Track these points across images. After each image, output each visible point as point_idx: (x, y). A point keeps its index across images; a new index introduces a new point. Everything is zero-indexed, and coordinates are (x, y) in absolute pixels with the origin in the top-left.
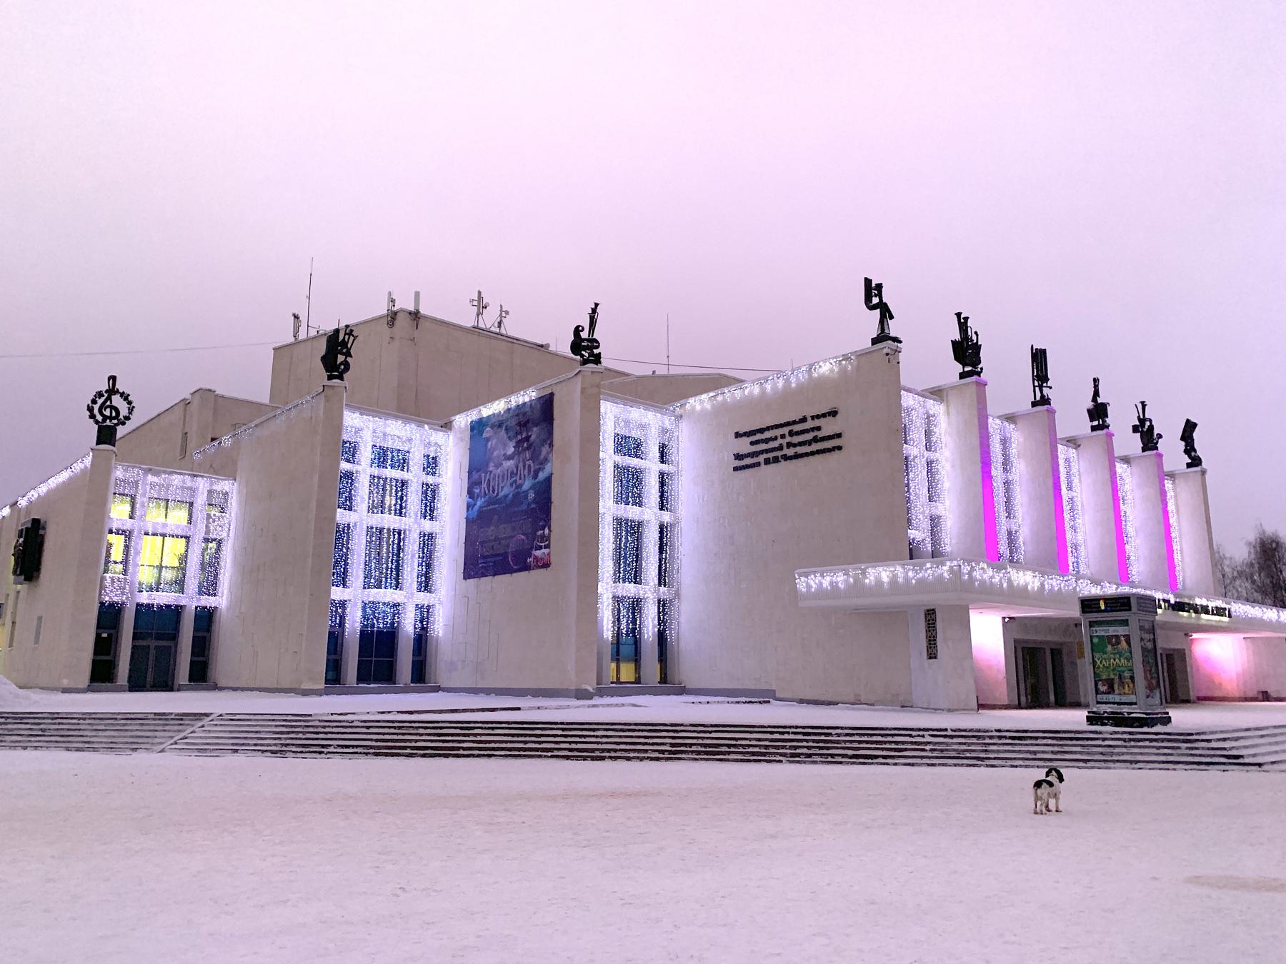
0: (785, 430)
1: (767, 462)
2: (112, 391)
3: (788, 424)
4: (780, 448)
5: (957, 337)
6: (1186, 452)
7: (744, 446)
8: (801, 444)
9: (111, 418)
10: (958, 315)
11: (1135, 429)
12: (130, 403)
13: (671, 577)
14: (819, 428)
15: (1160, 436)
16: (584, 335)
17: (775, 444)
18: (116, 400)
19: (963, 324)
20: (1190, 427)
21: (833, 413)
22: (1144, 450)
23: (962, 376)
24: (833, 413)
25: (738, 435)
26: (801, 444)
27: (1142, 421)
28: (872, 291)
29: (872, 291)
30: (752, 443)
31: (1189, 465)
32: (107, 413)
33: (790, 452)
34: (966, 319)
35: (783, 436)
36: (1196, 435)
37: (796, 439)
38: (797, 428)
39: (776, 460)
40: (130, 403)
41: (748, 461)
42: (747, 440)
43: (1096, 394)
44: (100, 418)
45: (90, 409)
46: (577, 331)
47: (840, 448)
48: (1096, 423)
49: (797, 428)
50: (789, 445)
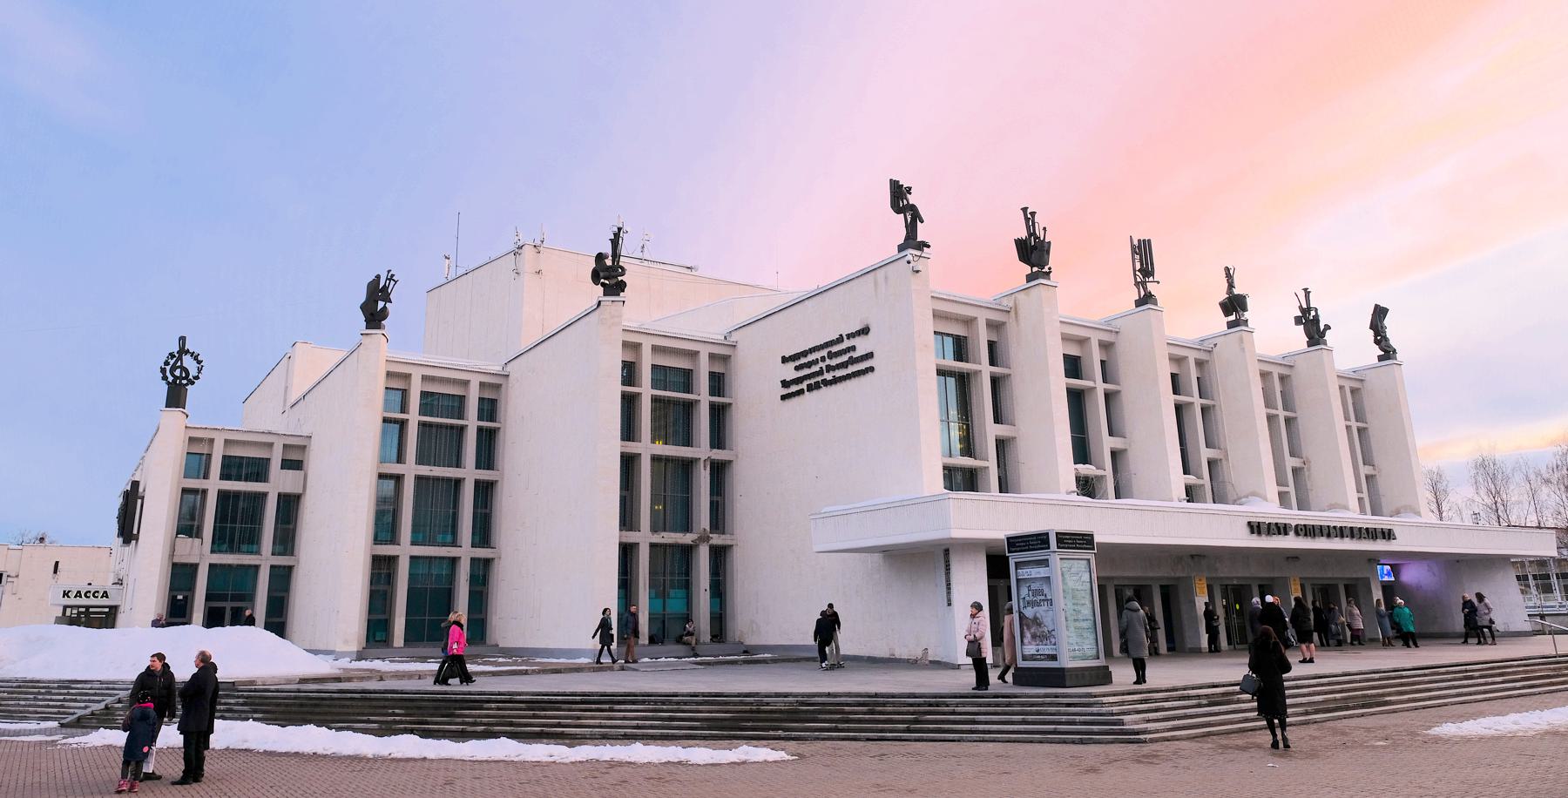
0: (824, 353)
1: (810, 388)
2: (183, 351)
3: (827, 345)
4: (820, 372)
5: (1023, 234)
6: (1377, 342)
7: (789, 372)
8: (839, 366)
9: (181, 378)
10: (1025, 210)
11: (1298, 321)
12: (199, 362)
13: (1312, 496)
14: (853, 348)
15: (1327, 327)
16: (609, 262)
17: (815, 369)
18: (188, 361)
19: (1029, 217)
20: (1380, 313)
21: (865, 331)
22: (1310, 344)
23: (1030, 278)
24: (865, 331)
25: (785, 360)
26: (839, 366)
27: (1306, 311)
28: (898, 193)
29: (898, 193)
30: (797, 368)
31: (1381, 358)
32: (177, 373)
33: (828, 376)
34: (1033, 214)
35: (823, 359)
36: (1387, 322)
37: (834, 362)
38: (835, 349)
39: (817, 386)
40: (199, 362)
41: (794, 388)
42: (792, 365)
43: (1231, 286)
44: (171, 379)
45: (163, 371)
46: (600, 257)
47: (871, 369)
48: (1233, 318)
49: (835, 349)
50: (829, 368)
